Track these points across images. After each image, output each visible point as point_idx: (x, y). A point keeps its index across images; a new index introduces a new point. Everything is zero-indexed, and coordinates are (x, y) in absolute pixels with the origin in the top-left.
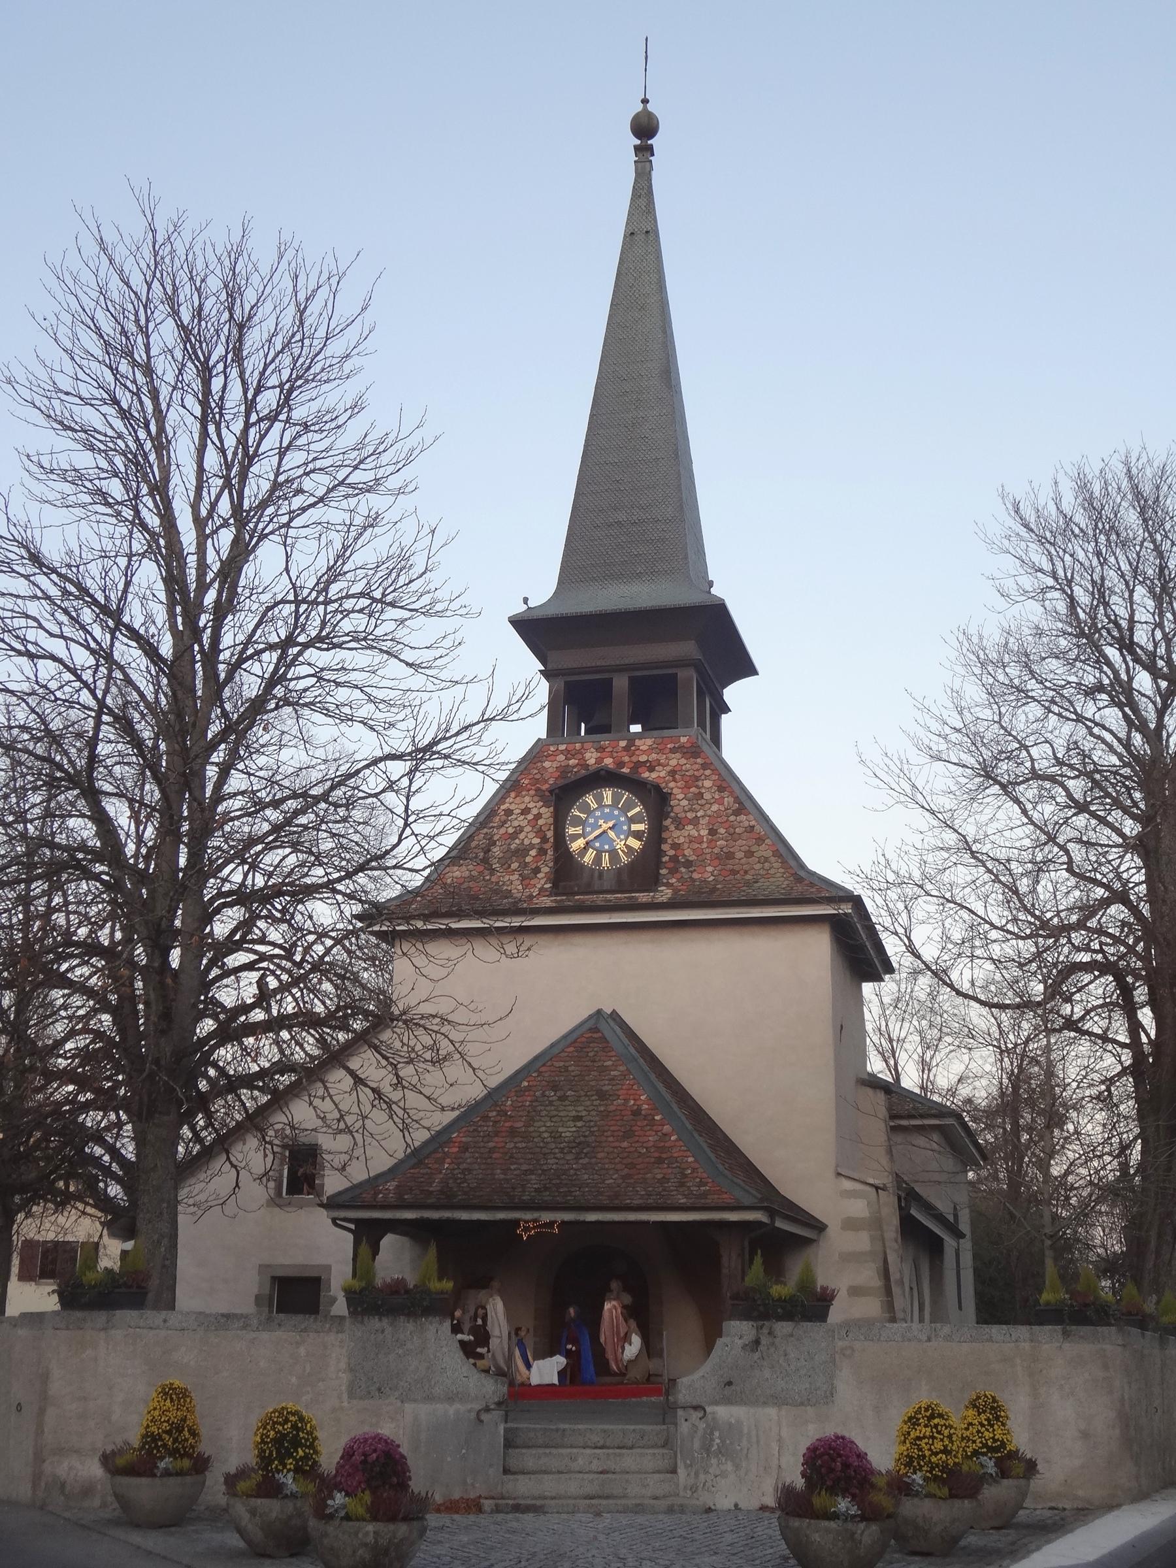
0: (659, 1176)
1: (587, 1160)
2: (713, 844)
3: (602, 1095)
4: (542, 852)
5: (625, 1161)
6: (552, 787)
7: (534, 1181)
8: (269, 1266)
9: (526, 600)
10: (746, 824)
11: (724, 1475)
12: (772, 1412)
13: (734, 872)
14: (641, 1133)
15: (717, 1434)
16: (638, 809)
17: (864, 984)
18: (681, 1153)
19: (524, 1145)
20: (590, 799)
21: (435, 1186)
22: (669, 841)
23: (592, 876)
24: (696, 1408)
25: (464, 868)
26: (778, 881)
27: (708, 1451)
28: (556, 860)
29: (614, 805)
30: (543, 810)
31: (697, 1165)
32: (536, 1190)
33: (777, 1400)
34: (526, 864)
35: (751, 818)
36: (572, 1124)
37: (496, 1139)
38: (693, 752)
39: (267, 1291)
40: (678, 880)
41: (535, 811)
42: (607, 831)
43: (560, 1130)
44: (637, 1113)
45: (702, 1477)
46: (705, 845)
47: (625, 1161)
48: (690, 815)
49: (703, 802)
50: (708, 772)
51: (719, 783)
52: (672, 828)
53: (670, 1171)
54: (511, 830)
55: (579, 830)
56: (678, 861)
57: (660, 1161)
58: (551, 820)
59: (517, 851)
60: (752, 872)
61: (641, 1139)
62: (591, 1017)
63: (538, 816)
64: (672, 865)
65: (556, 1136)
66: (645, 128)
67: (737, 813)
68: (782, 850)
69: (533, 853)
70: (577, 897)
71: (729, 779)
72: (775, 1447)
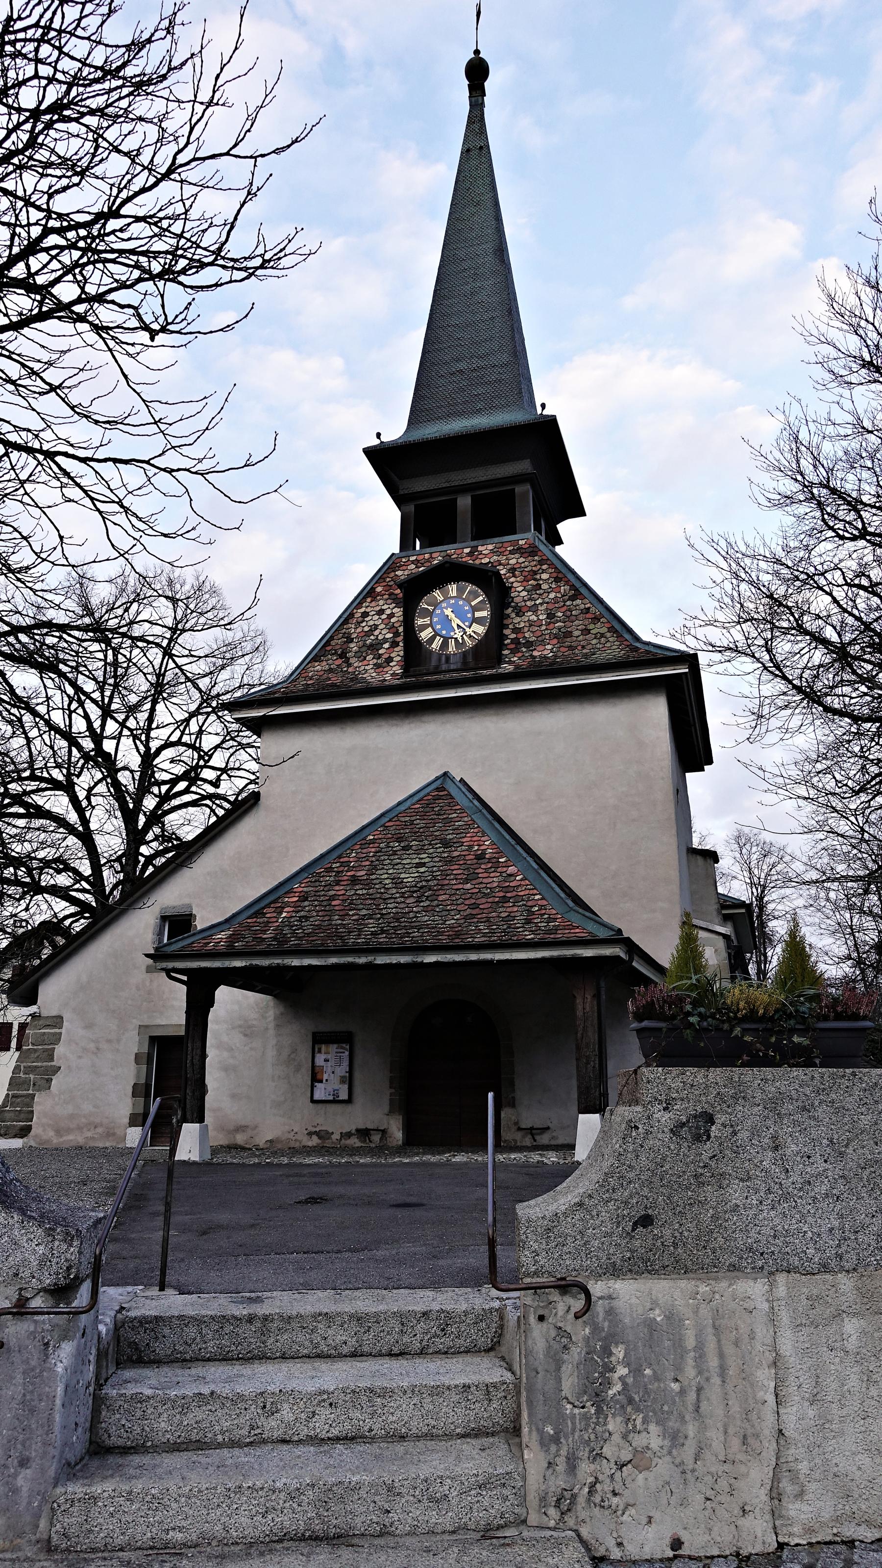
0: (503, 915)
1: (428, 903)
2: (551, 626)
3: (446, 844)
4: (394, 644)
5: (467, 902)
6: (405, 588)
7: (372, 925)
8: (147, 1027)
9: (378, 435)
10: (582, 606)
11: (640, 1460)
12: (755, 1289)
13: (571, 648)
14: (485, 875)
15: (619, 1352)
16: (481, 598)
17: (688, 775)
18: (527, 892)
19: (365, 892)
20: (437, 594)
21: (269, 935)
22: (511, 626)
23: (440, 660)
24: (565, 1287)
25: (325, 663)
26: (613, 650)
27: (598, 1399)
28: (406, 649)
29: (459, 596)
30: (396, 610)
31: (544, 902)
32: (373, 933)
33: (768, 1263)
34: (380, 656)
35: (586, 601)
36: (414, 870)
37: (337, 888)
38: (531, 551)
39: (145, 1049)
40: (519, 658)
41: (388, 612)
42: (455, 619)
43: (402, 876)
44: (480, 857)
45: (585, 1469)
46: (544, 628)
47: (467, 902)
48: (529, 603)
49: (541, 591)
50: (545, 567)
51: (555, 575)
52: (513, 615)
53: (515, 909)
54: (366, 629)
55: (427, 621)
56: (519, 643)
57: (505, 900)
58: (401, 619)
59: (371, 645)
60: (590, 646)
61: (485, 881)
62: (437, 779)
63: (392, 615)
64: (513, 646)
65: (398, 882)
66: (477, 72)
67: (573, 598)
68: (618, 626)
69: (386, 645)
70: (426, 684)
71: (564, 570)
72: (765, 1377)
